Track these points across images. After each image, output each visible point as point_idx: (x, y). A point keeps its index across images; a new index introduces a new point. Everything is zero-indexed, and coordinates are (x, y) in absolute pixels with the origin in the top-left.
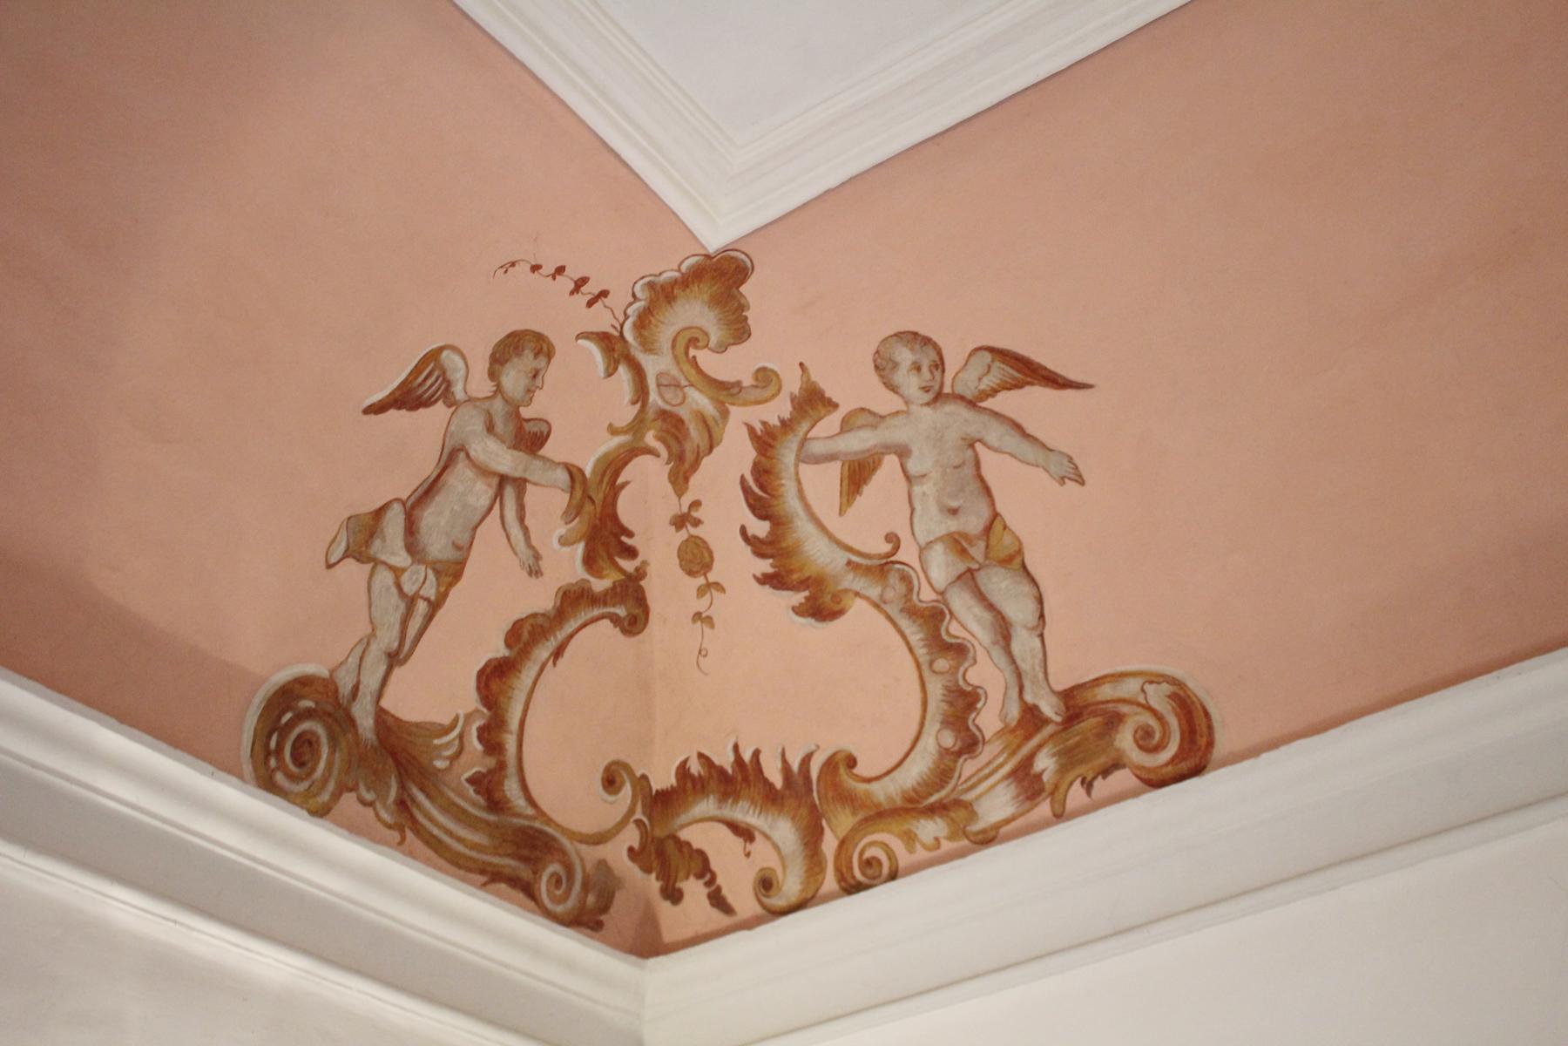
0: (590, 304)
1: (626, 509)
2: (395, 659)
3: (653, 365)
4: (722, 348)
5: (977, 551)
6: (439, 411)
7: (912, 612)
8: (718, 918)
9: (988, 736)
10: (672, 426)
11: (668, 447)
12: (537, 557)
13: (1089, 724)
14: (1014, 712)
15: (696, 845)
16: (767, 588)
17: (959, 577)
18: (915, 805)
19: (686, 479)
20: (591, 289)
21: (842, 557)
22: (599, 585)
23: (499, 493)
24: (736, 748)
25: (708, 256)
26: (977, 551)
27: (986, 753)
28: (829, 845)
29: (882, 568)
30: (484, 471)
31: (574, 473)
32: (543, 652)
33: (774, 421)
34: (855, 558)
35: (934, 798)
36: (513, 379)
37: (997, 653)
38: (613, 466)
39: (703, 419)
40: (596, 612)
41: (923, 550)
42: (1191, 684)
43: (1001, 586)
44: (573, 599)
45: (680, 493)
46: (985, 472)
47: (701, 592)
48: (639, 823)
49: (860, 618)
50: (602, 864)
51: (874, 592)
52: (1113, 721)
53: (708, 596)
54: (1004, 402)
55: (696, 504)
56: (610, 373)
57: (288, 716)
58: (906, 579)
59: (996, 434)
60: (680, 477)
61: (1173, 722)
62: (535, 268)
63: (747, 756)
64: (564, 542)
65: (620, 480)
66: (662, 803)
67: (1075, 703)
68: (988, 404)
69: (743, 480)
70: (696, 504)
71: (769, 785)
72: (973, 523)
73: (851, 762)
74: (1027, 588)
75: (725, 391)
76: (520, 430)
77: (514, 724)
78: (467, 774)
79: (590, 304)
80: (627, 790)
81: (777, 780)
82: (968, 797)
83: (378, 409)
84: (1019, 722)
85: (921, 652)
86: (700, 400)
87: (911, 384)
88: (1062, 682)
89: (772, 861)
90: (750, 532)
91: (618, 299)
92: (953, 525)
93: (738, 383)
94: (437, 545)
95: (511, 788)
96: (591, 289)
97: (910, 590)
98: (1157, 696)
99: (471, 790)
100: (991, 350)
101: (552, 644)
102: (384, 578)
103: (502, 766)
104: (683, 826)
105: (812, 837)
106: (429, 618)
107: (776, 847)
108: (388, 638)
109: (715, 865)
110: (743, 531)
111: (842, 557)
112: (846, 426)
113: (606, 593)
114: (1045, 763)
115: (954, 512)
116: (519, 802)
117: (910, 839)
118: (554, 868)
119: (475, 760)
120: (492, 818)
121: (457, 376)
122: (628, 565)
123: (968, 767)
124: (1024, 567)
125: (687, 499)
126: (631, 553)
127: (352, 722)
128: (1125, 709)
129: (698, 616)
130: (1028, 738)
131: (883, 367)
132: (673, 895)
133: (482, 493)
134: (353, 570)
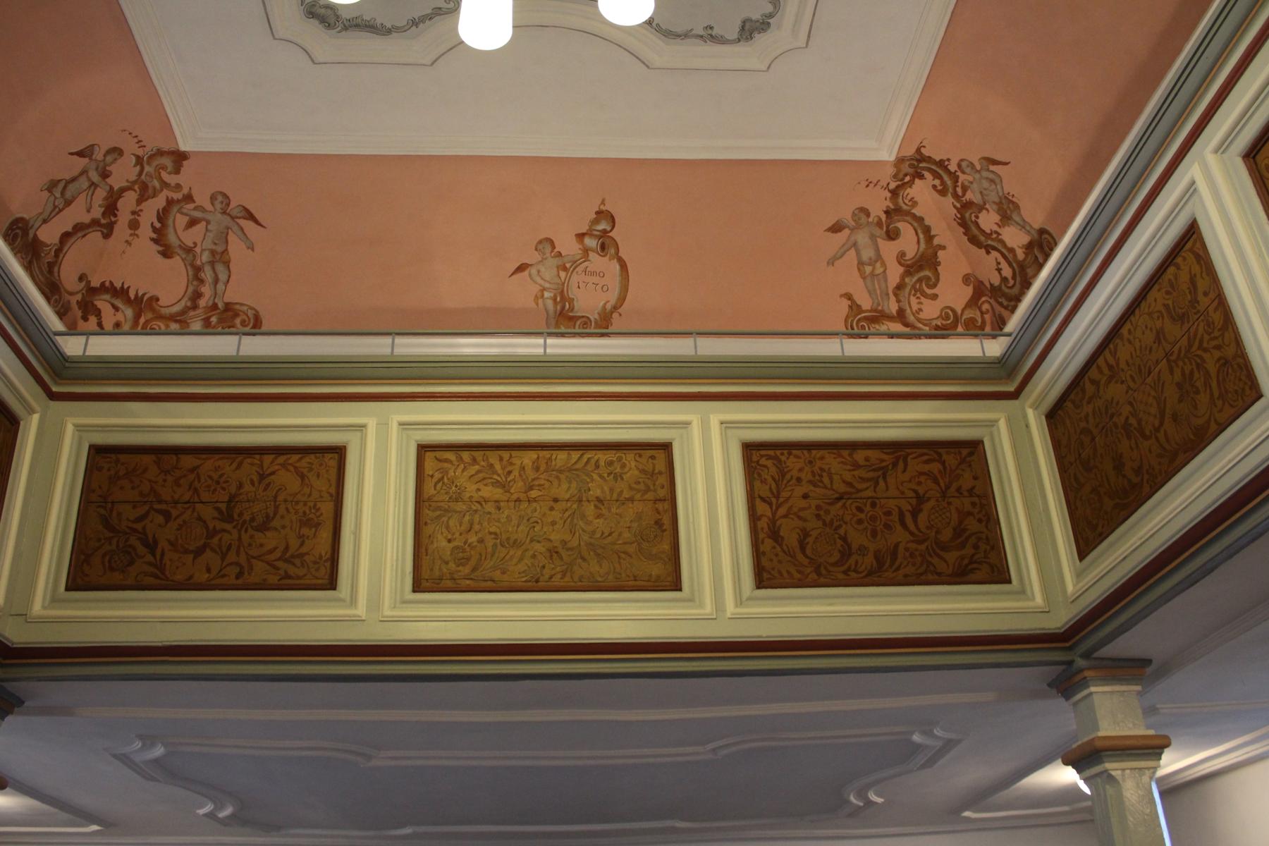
0: (139, 147)
1: (120, 204)
2: (45, 221)
3: (147, 169)
4: (170, 173)
5: (218, 257)
6: (86, 160)
7: (192, 265)
8: (97, 329)
9: (201, 306)
10: (144, 187)
11: (140, 191)
12: (91, 207)
13: (230, 313)
14: (210, 303)
15: (98, 307)
16: (152, 242)
17: (210, 262)
18: (172, 318)
19: (142, 202)
20: (142, 144)
21: (178, 243)
22: (103, 221)
23: (90, 186)
24: (123, 284)
25: (178, 150)
26: (218, 257)
27: (197, 312)
28: (142, 320)
29: (189, 250)
30: (89, 179)
31: (111, 188)
32: (80, 234)
33: (175, 198)
34: (182, 245)
35: (178, 318)
36: (109, 159)
37: (212, 286)
38: (123, 190)
39: (154, 188)
40: (99, 228)
41: (203, 250)
42: (261, 314)
43: (220, 268)
44: (95, 222)
45: (137, 206)
46: (229, 237)
47: (131, 235)
48: (83, 294)
49: (177, 262)
50: (69, 302)
51: (184, 256)
52: (236, 315)
53: (132, 238)
54: (242, 222)
55: (141, 210)
56: (135, 166)
57: (15, 227)
58: (194, 256)
59: (235, 228)
60: (140, 201)
61: (252, 321)
62: (130, 134)
63: (126, 287)
64: (100, 206)
65: (123, 195)
66: (93, 291)
67: (228, 307)
68: (237, 220)
69: (159, 209)
70: (141, 210)
71: (129, 298)
72: (220, 249)
73: (158, 300)
74: (227, 272)
75: (165, 185)
76: (103, 172)
77: (64, 252)
78: (47, 261)
79: (139, 147)
80: (84, 283)
81: (132, 297)
82: (189, 321)
83: (72, 154)
84: (211, 306)
85: (191, 277)
86: (156, 183)
87: (218, 206)
88: (226, 300)
89: (122, 319)
90: (154, 224)
91: (147, 149)
92: (214, 247)
93: (170, 184)
94: (68, 195)
95: (56, 269)
96: (136, 140)
97: (194, 259)
98: (250, 313)
99: (46, 265)
100: (244, 207)
101: (83, 233)
102: (52, 198)
103: (56, 262)
104: (96, 300)
105: (137, 317)
106: (58, 213)
107: (125, 316)
108: (45, 215)
109: (103, 314)
110: (152, 223)
111: (178, 243)
112: (196, 208)
113: (104, 224)
114: (214, 320)
115: (215, 244)
116: (56, 274)
117: (167, 326)
118: (57, 297)
119: (50, 258)
120: (48, 276)
121: (96, 153)
122: (113, 219)
123: (192, 313)
124: (228, 266)
125: (139, 208)
126: (115, 216)
127: (28, 234)
128: (241, 313)
129: (127, 241)
130: (212, 311)
131: (213, 198)
132: (85, 319)
133: (86, 185)
134: (46, 194)
